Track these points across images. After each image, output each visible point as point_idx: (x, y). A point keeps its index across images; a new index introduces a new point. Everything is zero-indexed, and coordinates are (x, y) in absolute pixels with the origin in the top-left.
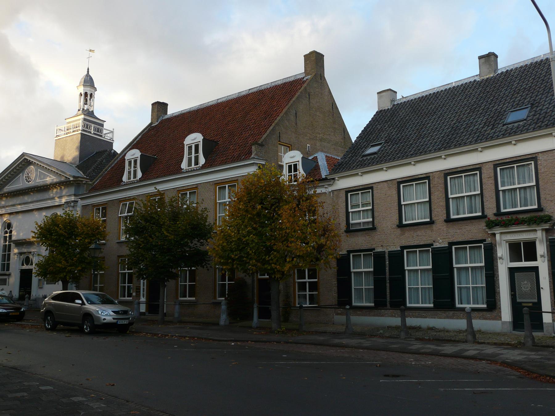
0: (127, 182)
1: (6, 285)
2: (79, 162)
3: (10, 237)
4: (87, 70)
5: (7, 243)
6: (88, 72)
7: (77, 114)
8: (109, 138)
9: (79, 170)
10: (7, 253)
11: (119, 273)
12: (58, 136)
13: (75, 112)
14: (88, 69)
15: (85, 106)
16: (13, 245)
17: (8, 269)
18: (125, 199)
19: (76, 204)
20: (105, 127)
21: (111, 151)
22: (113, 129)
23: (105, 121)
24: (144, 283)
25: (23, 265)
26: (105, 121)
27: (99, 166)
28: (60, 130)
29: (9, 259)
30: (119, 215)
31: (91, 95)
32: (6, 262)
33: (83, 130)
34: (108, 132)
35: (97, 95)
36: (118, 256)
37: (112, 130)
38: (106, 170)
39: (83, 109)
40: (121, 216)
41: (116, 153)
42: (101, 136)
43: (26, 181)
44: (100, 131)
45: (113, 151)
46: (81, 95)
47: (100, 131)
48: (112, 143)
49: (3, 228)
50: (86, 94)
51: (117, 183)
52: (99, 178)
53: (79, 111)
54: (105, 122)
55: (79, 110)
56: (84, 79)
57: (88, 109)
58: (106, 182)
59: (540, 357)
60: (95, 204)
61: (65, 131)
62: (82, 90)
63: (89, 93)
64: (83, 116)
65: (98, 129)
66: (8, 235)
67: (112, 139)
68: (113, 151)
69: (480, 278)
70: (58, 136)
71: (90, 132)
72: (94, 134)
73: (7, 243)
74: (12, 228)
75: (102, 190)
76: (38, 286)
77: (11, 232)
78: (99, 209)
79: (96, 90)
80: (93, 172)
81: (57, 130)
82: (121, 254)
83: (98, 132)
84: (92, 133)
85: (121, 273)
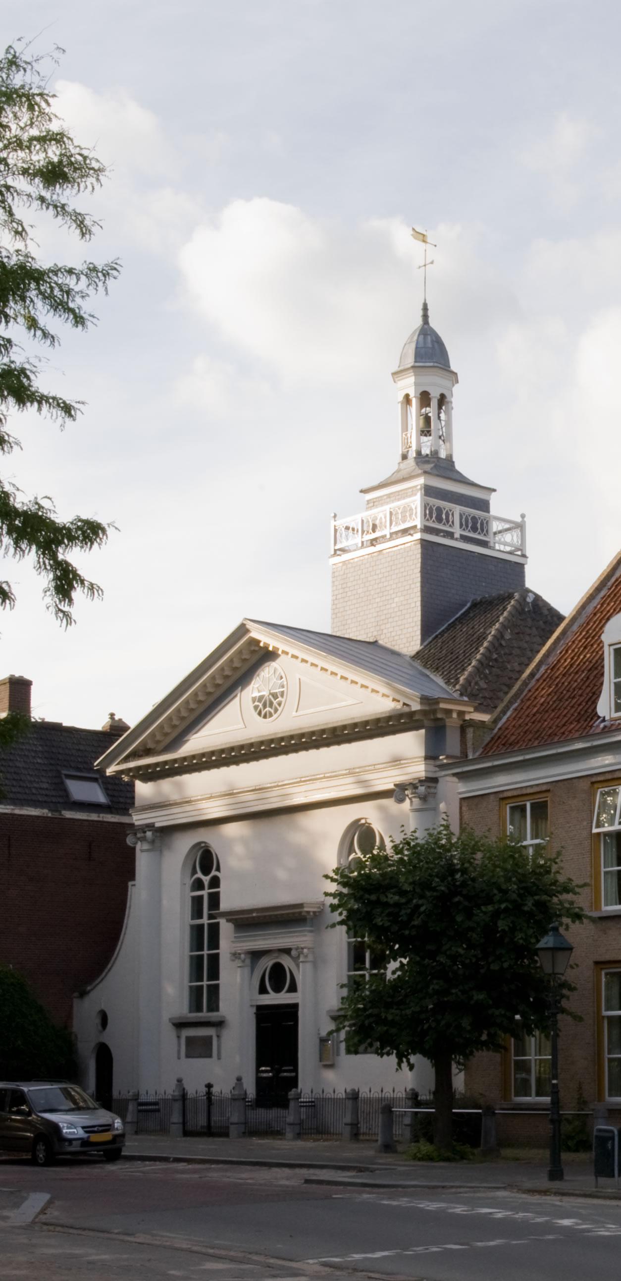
0: (611, 720)
1: (210, 1056)
2: (421, 644)
3: (215, 900)
4: (421, 313)
5: (205, 921)
6: (425, 317)
7: (398, 471)
8: (508, 549)
9: (428, 672)
10: (206, 952)
11: (600, 1018)
12: (343, 550)
13: (390, 464)
14: (425, 308)
15: (424, 439)
16: (226, 928)
17: (214, 1005)
18: (609, 777)
19: (432, 790)
20: (494, 510)
21: (525, 599)
22: (523, 516)
23: (494, 490)
24: (396, 1131)
25: (263, 990)
26: (494, 490)
27: (495, 656)
28: (347, 528)
29: (214, 973)
30: (595, 831)
31: (442, 400)
32: (205, 983)
33: (427, 529)
34: (507, 526)
35: (458, 396)
36: (597, 963)
37: (519, 520)
38: (532, 675)
39: (419, 453)
40: (599, 834)
41: (540, 603)
42: (484, 544)
43: (255, 715)
44: (482, 524)
45: (530, 599)
46: (407, 399)
47: (482, 524)
48: (521, 566)
49: (189, 871)
50: (425, 398)
51: (578, 721)
52: (511, 703)
53: (406, 462)
54: (493, 493)
55: (404, 457)
56: (413, 346)
57: (435, 453)
58: (538, 716)
59: (519, 701)
60: (509, 794)
61: (363, 532)
62: (409, 385)
63: (435, 395)
64: (421, 481)
65: (474, 519)
66: (205, 893)
67: (521, 550)
68: (530, 599)
69: (217, 810)
70: (343, 550)
71: (450, 535)
72: (464, 538)
73: (205, 921)
74: (218, 869)
75: (530, 749)
76: (321, 1061)
77: (215, 882)
78: (523, 809)
79: (454, 377)
80: (477, 679)
81: (336, 531)
82: (607, 957)
83: (474, 529)
84: (457, 535)
85: (610, 1018)
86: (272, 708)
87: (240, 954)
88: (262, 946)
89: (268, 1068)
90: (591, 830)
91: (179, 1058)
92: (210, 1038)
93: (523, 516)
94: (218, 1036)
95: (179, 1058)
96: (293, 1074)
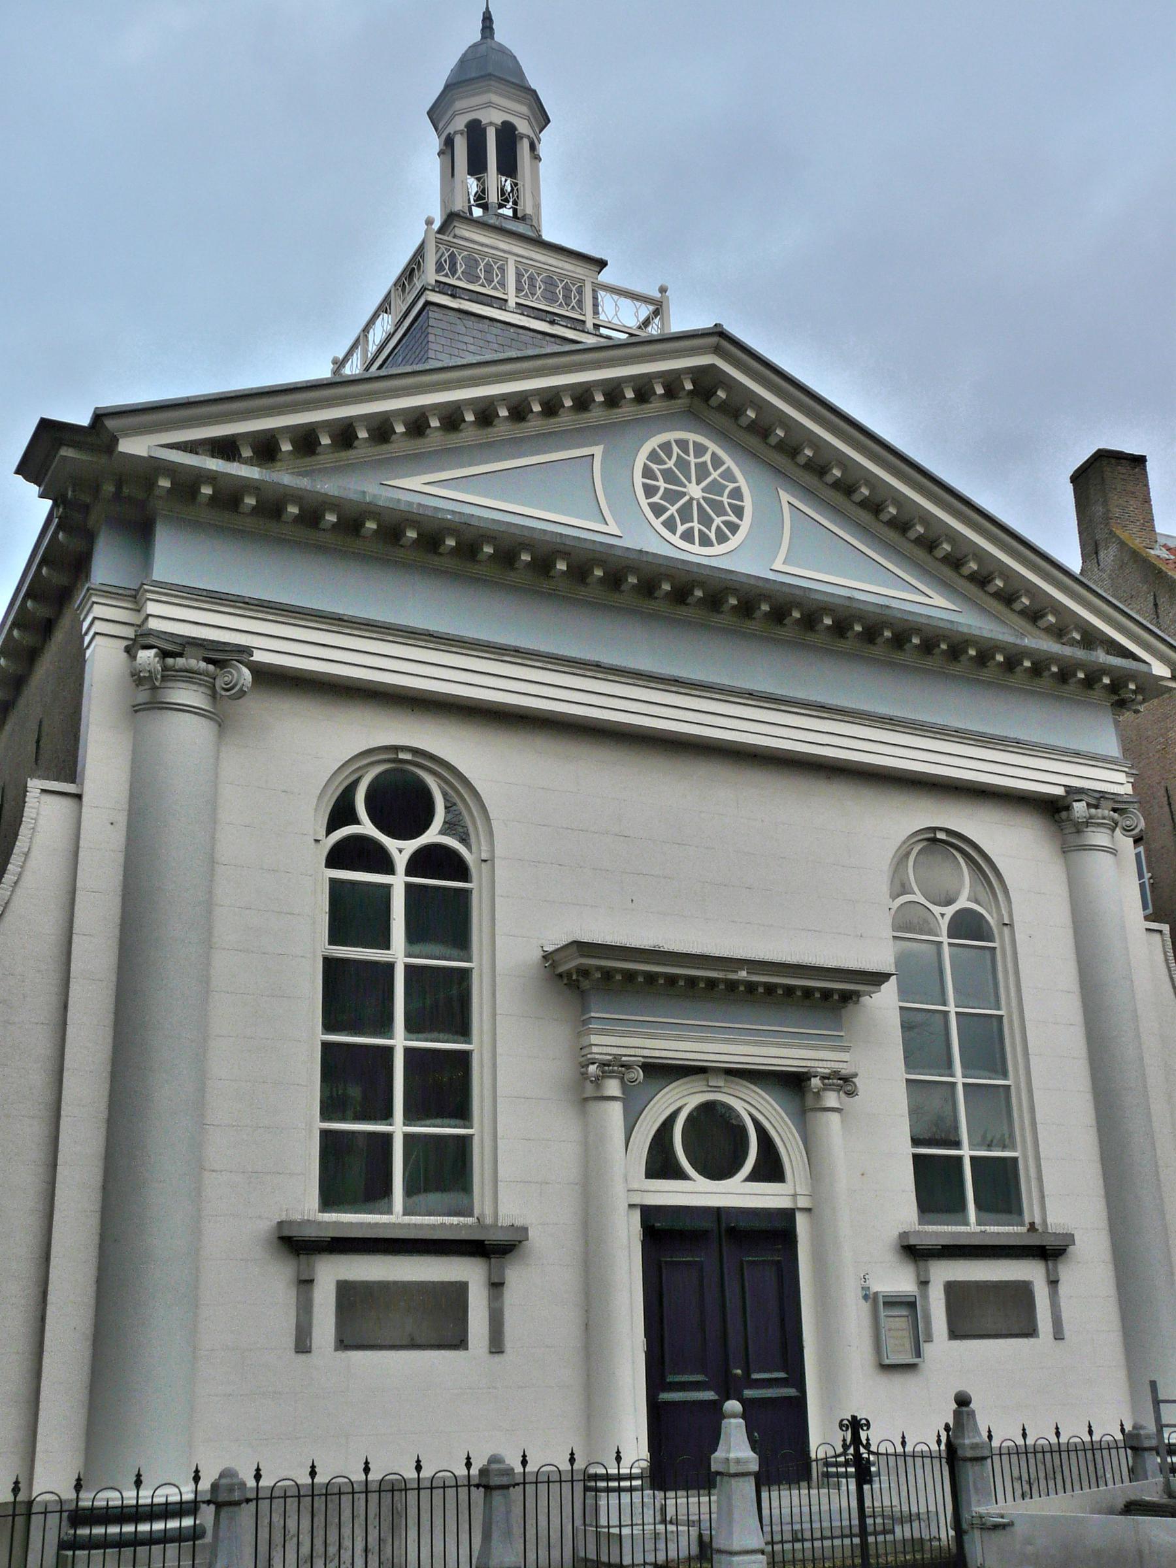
22: (663, 290)
72: (522, 308)
84: (512, 303)
86: (726, 514)
87: (627, 1066)
88: (657, 1054)
89: (782, 1375)
90: (1146, 850)
91: (303, 1345)
92: (459, 1291)
93: (663, 290)
94: (1053, 1283)
95: (303, 1345)
96: (791, 1392)
